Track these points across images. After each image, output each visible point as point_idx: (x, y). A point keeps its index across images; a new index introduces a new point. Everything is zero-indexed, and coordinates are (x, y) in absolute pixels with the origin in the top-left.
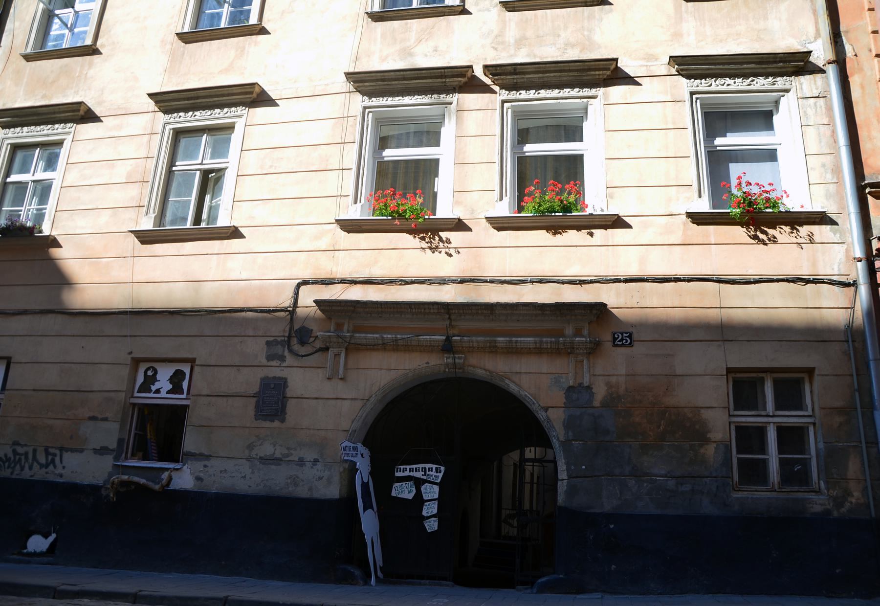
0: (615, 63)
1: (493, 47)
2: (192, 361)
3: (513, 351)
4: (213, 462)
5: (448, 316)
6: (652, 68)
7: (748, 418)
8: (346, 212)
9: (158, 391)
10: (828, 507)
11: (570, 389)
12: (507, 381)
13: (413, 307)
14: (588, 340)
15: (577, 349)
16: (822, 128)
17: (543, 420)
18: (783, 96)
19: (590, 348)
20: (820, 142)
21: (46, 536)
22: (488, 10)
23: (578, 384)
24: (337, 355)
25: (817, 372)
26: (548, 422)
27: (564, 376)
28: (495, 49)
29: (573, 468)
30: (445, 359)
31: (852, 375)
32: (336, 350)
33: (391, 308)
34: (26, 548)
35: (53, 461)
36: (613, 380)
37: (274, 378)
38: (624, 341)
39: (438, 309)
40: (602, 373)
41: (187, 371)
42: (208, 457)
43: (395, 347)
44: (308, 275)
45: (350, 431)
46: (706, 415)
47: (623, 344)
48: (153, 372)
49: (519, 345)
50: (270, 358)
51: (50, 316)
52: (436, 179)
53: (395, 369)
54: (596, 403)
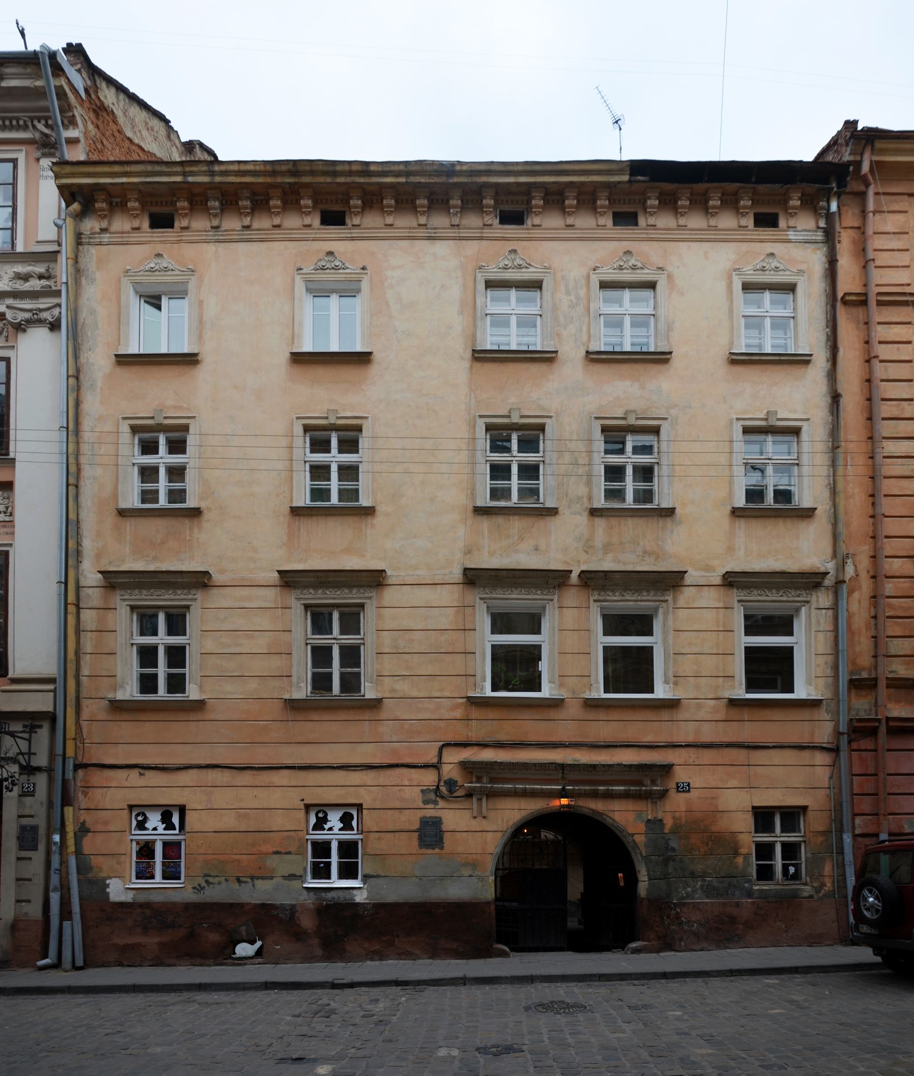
1: (585, 551)
2: (359, 807)
3: (609, 796)
6: (711, 579)
7: (765, 838)
8: (474, 689)
9: (330, 829)
10: (811, 893)
16: (828, 633)
18: (804, 606)
20: (826, 645)
21: (252, 942)
22: (580, 514)
24: (480, 800)
25: (810, 808)
28: (587, 552)
29: (652, 873)
31: (831, 810)
34: (235, 953)
36: (677, 814)
37: (431, 817)
40: (669, 810)
41: (355, 813)
44: (450, 738)
49: (613, 792)
50: (426, 802)
51: (249, 772)
52: (540, 662)
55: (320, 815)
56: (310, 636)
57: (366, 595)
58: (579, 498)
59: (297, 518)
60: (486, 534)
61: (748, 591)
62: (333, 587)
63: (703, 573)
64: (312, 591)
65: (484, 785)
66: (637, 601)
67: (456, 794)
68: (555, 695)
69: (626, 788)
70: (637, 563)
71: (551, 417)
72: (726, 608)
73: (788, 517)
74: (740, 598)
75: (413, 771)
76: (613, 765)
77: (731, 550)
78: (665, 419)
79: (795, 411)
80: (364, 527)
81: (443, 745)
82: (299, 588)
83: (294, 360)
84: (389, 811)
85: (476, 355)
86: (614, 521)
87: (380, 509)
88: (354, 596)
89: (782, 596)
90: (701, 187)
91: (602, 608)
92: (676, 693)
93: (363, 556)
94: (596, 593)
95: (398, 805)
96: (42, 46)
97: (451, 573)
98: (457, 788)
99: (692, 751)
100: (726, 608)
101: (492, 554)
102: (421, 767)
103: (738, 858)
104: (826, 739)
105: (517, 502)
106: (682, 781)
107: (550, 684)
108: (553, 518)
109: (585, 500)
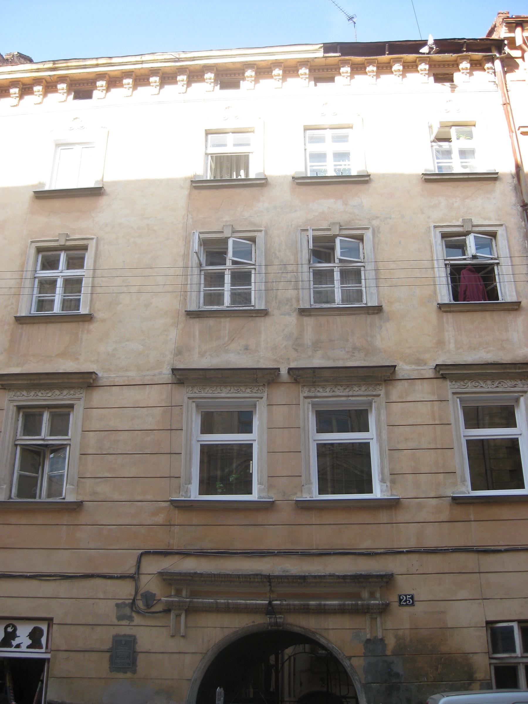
0: (393, 368)
1: (294, 349)
2: (50, 621)
5: (269, 584)
8: (178, 492)
9: (18, 646)
11: (368, 641)
12: (318, 636)
13: (241, 577)
14: (381, 602)
15: (372, 609)
17: (347, 666)
18: (522, 396)
19: (381, 609)
22: (289, 314)
23: (374, 637)
24: (178, 616)
26: (351, 668)
27: (362, 631)
28: (296, 350)
30: (268, 619)
33: (222, 578)
36: (400, 632)
37: (125, 636)
39: (261, 578)
43: (228, 609)
44: (149, 546)
45: (193, 680)
48: (13, 629)
49: (327, 607)
50: (120, 618)
52: (251, 462)
53: (227, 628)
54: (388, 653)
55: (10, 630)
56: (19, 437)
57: (77, 396)
58: (289, 300)
59: (20, 326)
60: (197, 336)
61: (462, 383)
62: (45, 389)
63: (413, 367)
64: (25, 393)
65: (182, 599)
66: (349, 396)
67: (153, 609)
68: (265, 498)
69: (340, 602)
70: (347, 359)
71: (261, 231)
72: (441, 401)
74: (455, 391)
75: (109, 582)
76: (324, 576)
77: (441, 343)
78: (367, 229)
79: (489, 219)
80: (80, 333)
81: (142, 554)
82: (13, 391)
83: (36, 197)
84: (80, 627)
85: (194, 185)
86: (323, 320)
87: (99, 315)
88: (65, 398)
89: (497, 387)
90: (386, 58)
91: (314, 405)
92: (395, 492)
93: (77, 359)
94: (306, 389)
95: (90, 621)
97: (160, 374)
98: (155, 602)
99: (414, 557)
100: (441, 401)
101: (202, 354)
102: (118, 578)
103: (473, 684)
105: (229, 306)
106: (406, 593)
107: (259, 486)
108: (262, 319)
109: (294, 301)
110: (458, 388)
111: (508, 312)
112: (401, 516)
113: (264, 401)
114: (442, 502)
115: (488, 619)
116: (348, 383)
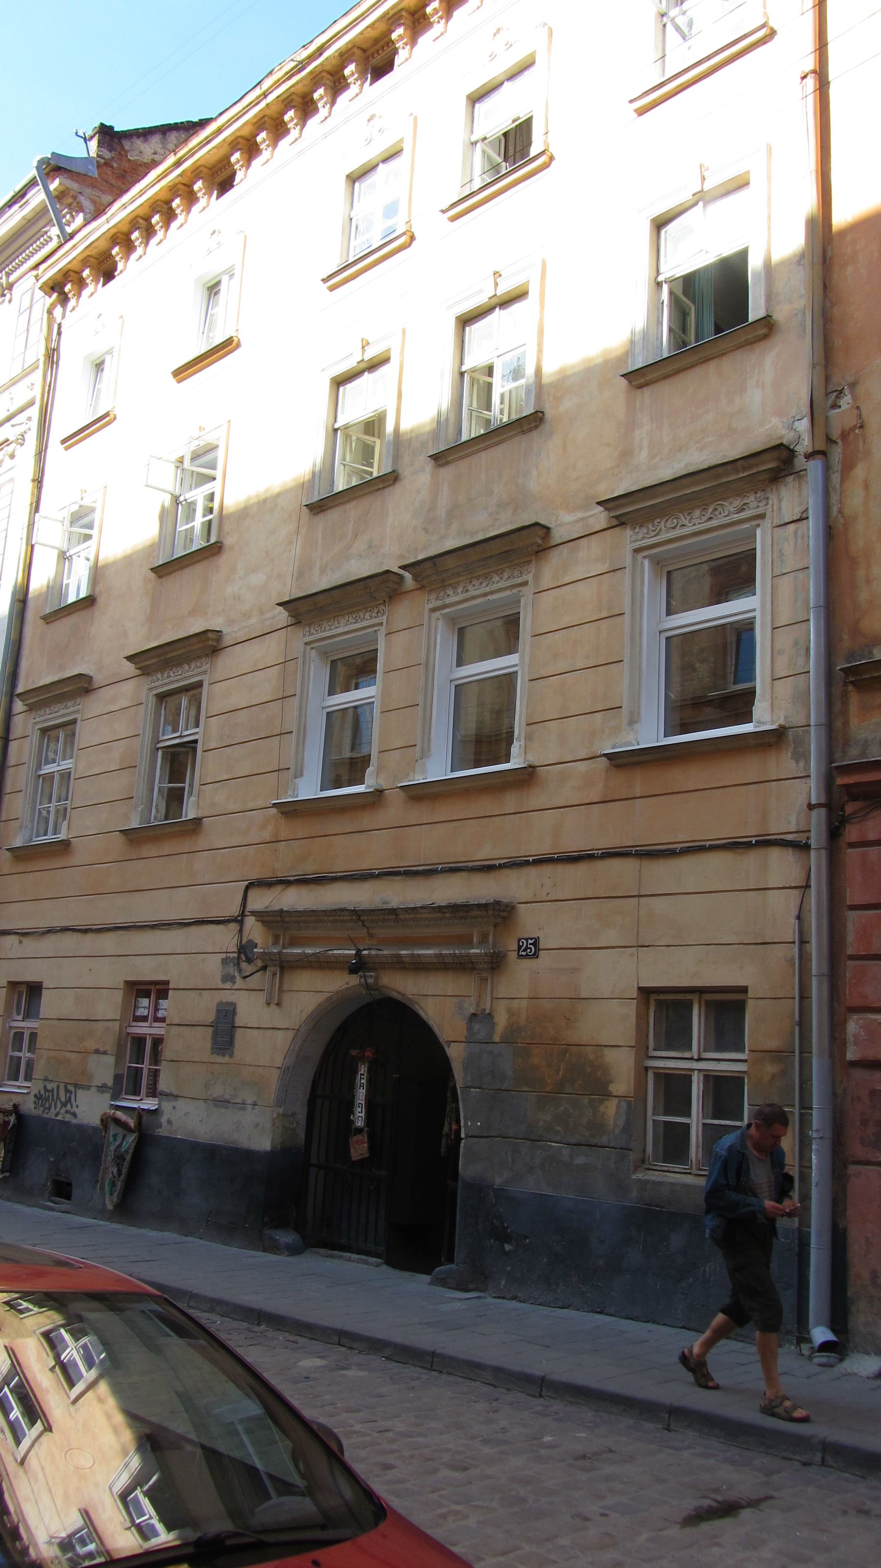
3: (419, 966)
4: (180, 1103)
12: (417, 1007)
18: (758, 525)
24: (274, 974)
32: (273, 969)
35: (70, 1098)
36: (515, 1004)
38: (529, 950)
42: (176, 1097)
46: (611, 1057)
47: (527, 955)
50: (228, 978)
57: (204, 668)
72: (614, 571)
73: (723, 355)
74: (637, 545)
89: (710, 519)
96: (53, 154)
104: (793, 820)
110: (643, 538)
111: (749, 347)
112: (536, 798)
113: (383, 630)
114: (595, 765)
115: (643, 984)
116: (487, 571)
